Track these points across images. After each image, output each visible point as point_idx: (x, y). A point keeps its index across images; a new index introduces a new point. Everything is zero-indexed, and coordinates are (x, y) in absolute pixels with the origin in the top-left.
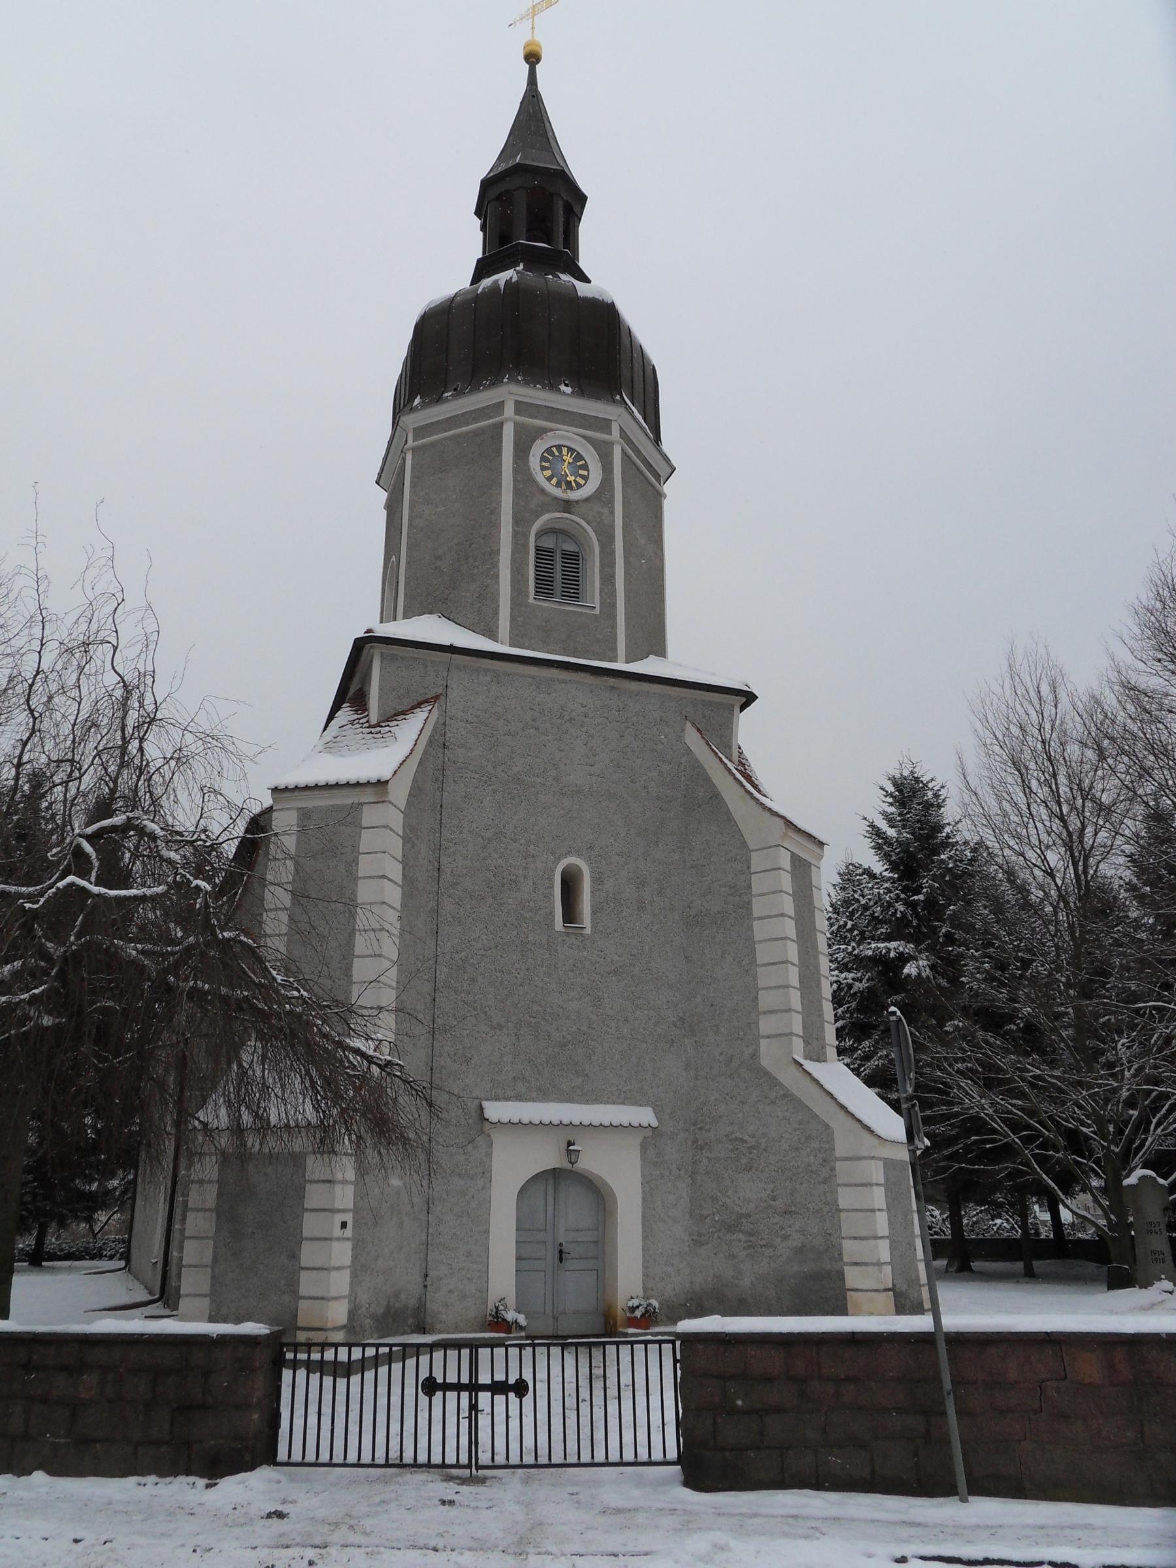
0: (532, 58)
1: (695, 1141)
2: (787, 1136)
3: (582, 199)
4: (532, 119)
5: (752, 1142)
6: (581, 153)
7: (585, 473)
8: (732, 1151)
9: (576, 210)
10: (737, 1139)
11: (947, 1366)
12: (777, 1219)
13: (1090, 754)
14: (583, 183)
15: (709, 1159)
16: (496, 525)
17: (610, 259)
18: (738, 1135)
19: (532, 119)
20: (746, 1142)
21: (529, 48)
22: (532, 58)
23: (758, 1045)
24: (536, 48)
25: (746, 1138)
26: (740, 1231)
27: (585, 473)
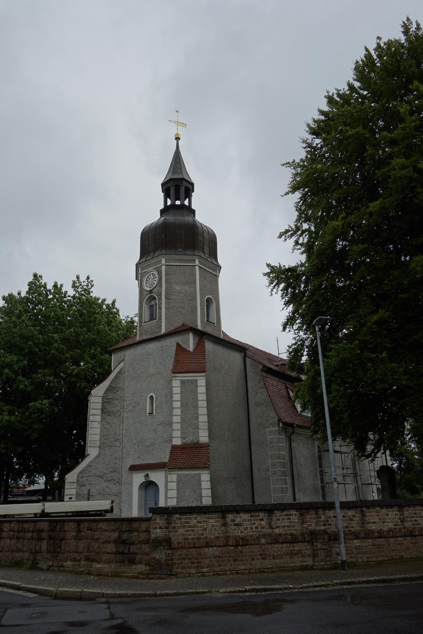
0: (178, 139)
19: (177, 161)
22: (178, 139)
24: (179, 137)
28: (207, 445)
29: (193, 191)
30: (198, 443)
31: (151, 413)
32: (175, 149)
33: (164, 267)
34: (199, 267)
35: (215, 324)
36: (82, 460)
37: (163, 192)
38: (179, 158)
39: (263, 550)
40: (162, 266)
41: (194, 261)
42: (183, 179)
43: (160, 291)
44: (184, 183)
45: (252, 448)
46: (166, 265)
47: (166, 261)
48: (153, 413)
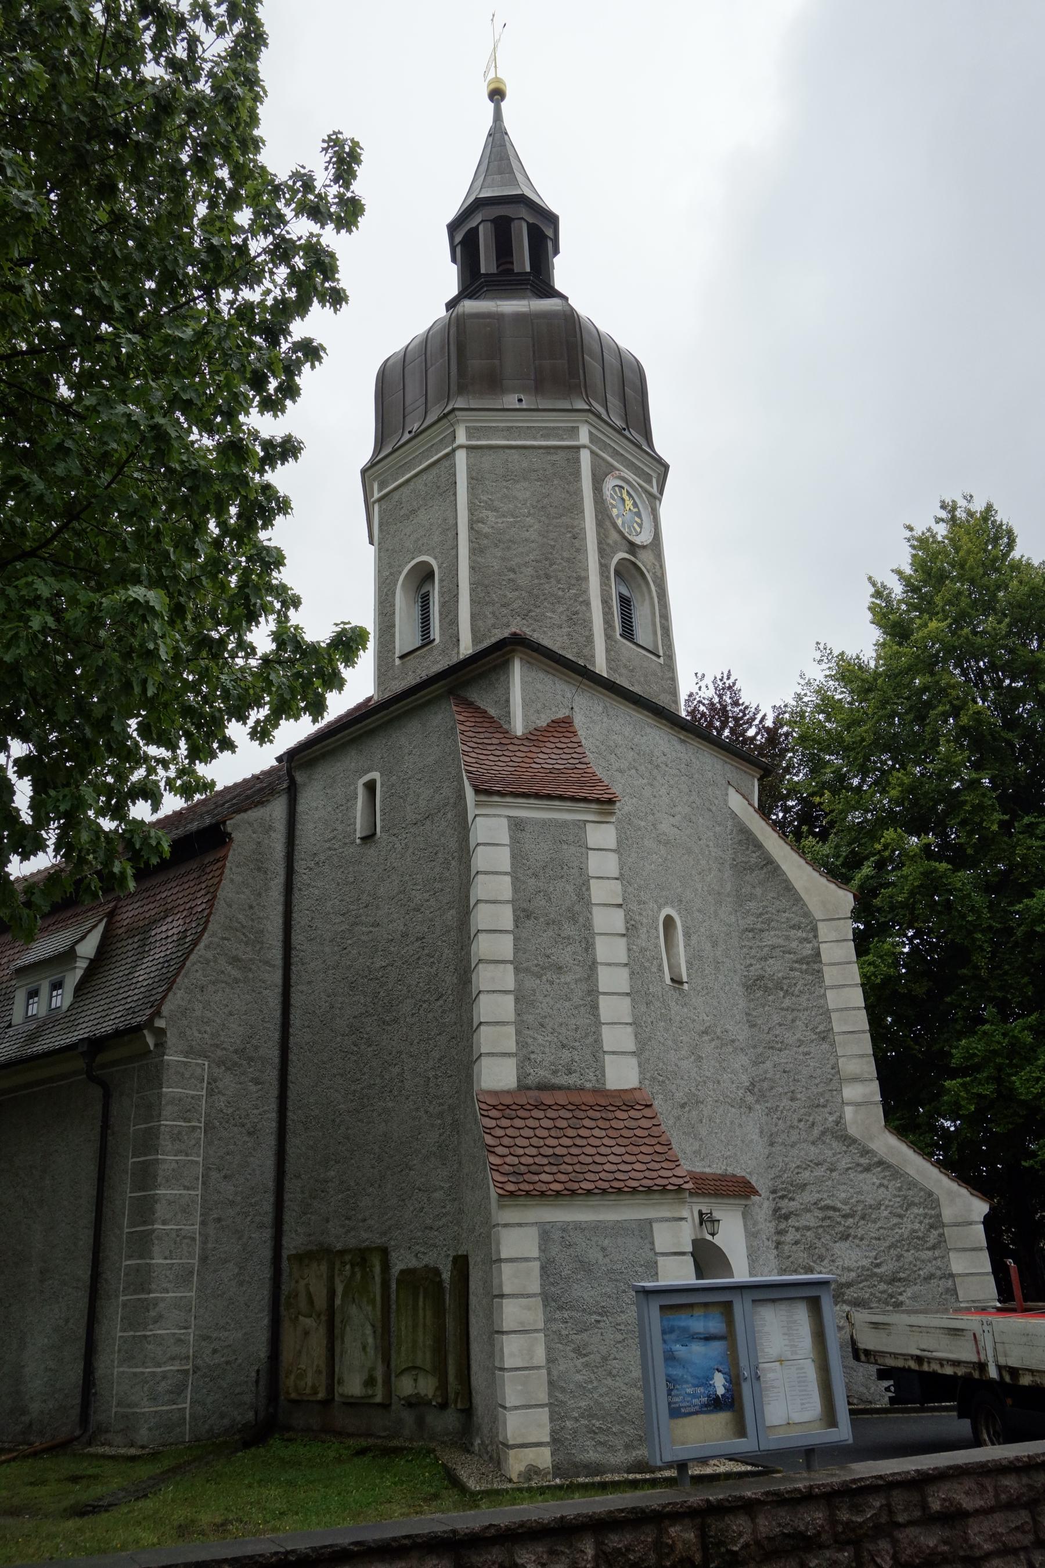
0: (497, 95)
1: (776, 1210)
2: (887, 1202)
3: (552, 219)
4: (498, 153)
5: (846, 1209)
6: (547, 183)
7: (638, 529)
8: (823, 1219)
9: (549, 233)
10: (828, 1208)
11: (1013, 1278)
12: (883, 1286)
13: (871, 695)
14: (551, 202)
15: (797, 1229)
16: (581, 549)
17: (586, 279)
18: (828, 1202)
19: (498, 153)
20: (839, 1210)
21: (492, 86)
22: (497, 95)
23: (843, 1112)
24: (502, 86)
25: (839, 1205)
26: (844, 1302)
27: (638, 529)
28: (507, 1201)
29: (556, 252)
30: (600, 1091)
31: (369, 838)
32: (489, 122)
33: (461, 457)
34: (592, 452)
35: (659, 657)
36: (940, 1165)
37: (454, 260)
38: (503, 145)
39: (28, 494)
40: (454, 450)
41: (574, 431)
42: (522, 200)
43: (451, 522)
44: (523, 212)
45: (270, 1163)
46: (469, 448)
47: (470, 433)
48: (375, 834)
